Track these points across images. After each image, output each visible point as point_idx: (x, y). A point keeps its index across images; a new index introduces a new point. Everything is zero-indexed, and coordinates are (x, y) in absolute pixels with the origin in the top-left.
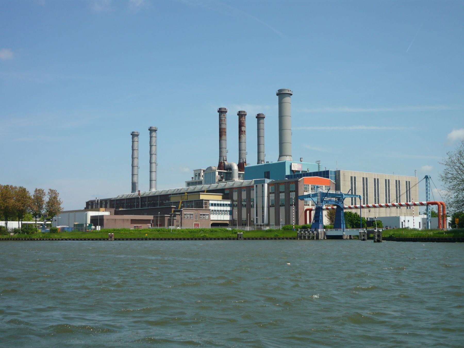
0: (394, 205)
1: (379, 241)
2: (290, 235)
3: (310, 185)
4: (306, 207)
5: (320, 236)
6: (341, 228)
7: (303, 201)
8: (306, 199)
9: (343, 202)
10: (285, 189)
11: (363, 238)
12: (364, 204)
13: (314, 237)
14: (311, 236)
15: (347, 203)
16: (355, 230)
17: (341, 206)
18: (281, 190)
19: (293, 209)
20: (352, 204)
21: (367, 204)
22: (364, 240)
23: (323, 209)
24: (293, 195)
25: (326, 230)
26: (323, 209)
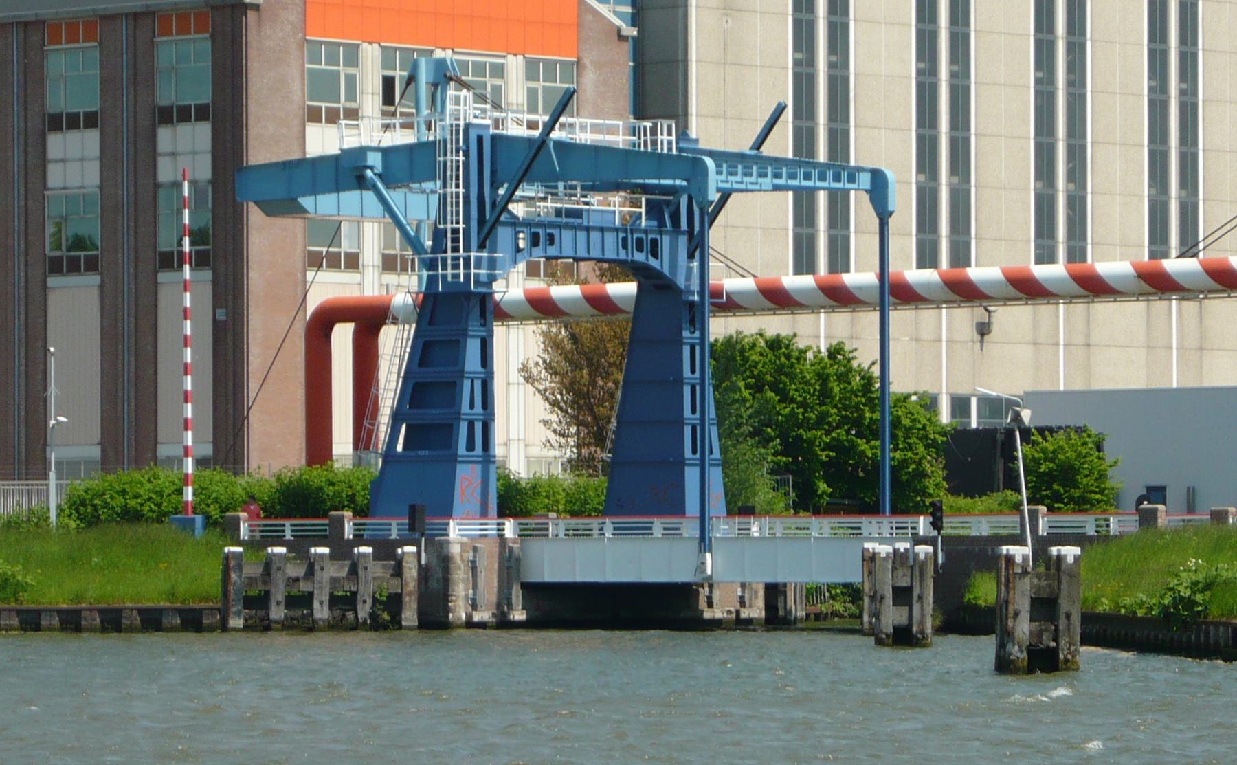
0: (1026, 289)
1: (1045, 661)
2: (145, 587)
3: (370, 54)
4: (327, 287)
5: (460, 592)
6: (678, 509)
7: (292, 226)
8: (322, 205)
9: (698, 246)
10: (108, 85)
11: (892, 616)
12: (1046, 256)
13: (394, 603)
14: (366, 592)
15: (750, 242)
16: (821, 527)
17: (684, 274)
18: (59, 101)
19: (186, 298)
20: (805, 263)
21: (1076, 253)
22: (904, 637)
23: (490, 311)
24: (185, 154)
25: (523, 534)
26: (490, 311)
